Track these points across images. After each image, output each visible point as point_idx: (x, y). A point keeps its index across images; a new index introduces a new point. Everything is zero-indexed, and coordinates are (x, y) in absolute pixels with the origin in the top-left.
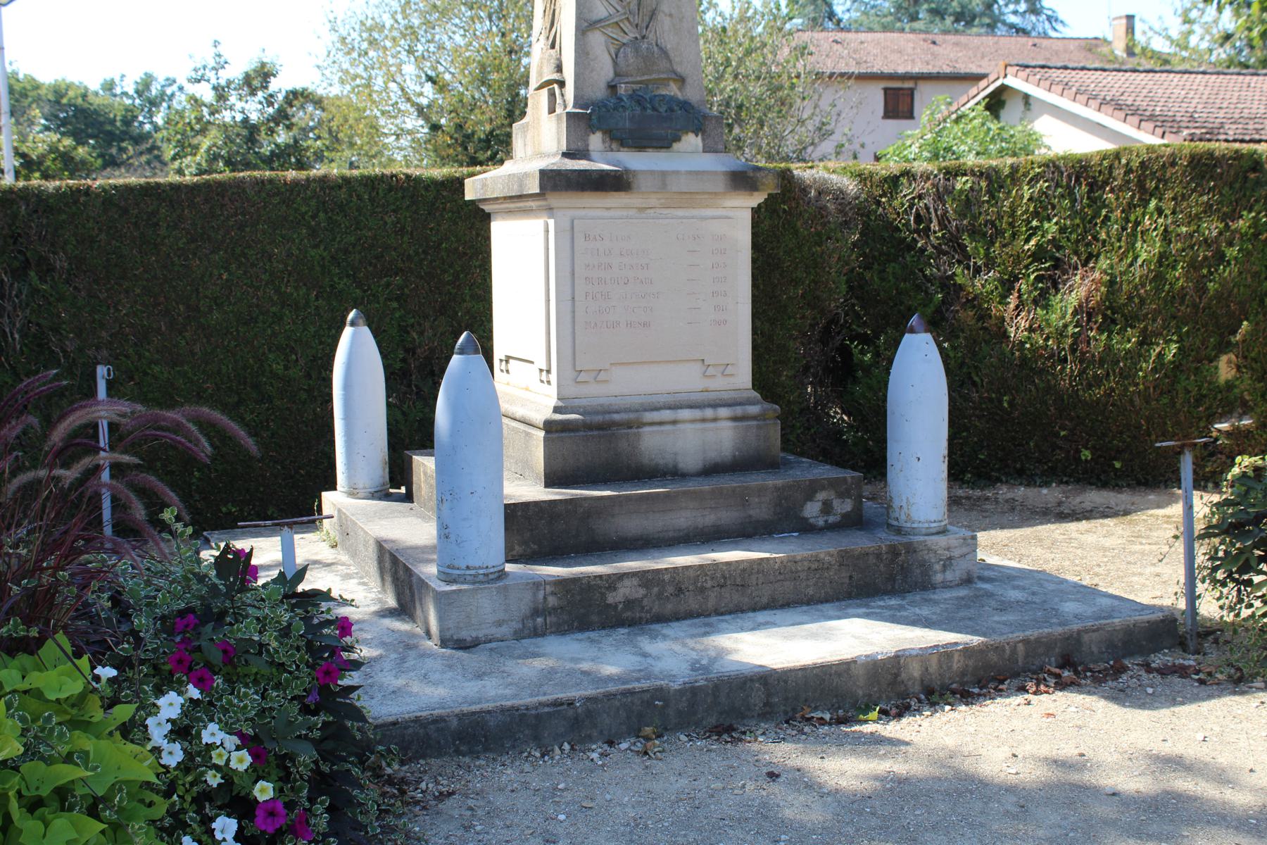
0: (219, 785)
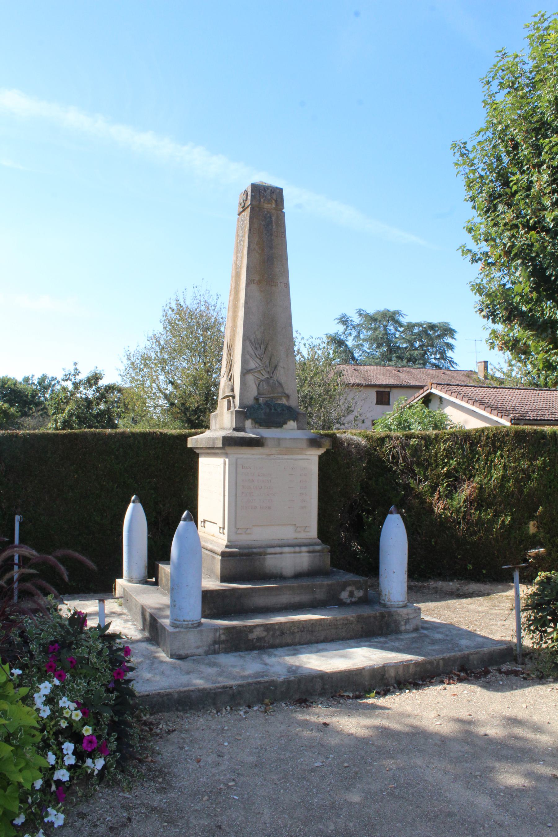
0: (66, 727)
